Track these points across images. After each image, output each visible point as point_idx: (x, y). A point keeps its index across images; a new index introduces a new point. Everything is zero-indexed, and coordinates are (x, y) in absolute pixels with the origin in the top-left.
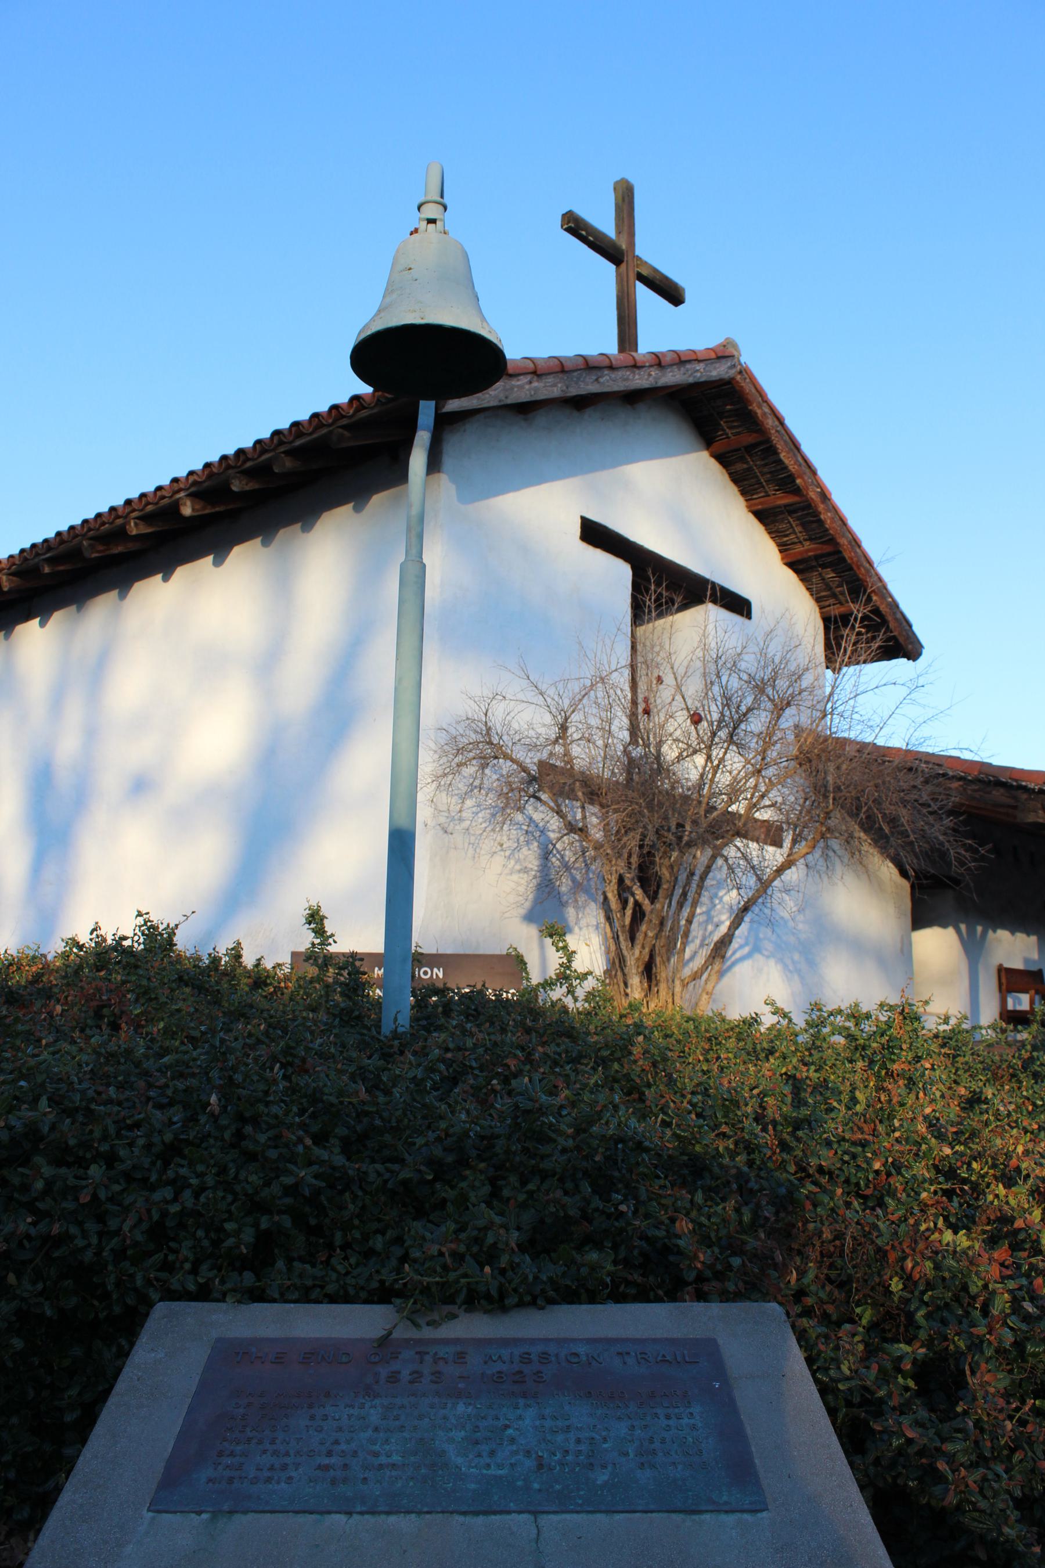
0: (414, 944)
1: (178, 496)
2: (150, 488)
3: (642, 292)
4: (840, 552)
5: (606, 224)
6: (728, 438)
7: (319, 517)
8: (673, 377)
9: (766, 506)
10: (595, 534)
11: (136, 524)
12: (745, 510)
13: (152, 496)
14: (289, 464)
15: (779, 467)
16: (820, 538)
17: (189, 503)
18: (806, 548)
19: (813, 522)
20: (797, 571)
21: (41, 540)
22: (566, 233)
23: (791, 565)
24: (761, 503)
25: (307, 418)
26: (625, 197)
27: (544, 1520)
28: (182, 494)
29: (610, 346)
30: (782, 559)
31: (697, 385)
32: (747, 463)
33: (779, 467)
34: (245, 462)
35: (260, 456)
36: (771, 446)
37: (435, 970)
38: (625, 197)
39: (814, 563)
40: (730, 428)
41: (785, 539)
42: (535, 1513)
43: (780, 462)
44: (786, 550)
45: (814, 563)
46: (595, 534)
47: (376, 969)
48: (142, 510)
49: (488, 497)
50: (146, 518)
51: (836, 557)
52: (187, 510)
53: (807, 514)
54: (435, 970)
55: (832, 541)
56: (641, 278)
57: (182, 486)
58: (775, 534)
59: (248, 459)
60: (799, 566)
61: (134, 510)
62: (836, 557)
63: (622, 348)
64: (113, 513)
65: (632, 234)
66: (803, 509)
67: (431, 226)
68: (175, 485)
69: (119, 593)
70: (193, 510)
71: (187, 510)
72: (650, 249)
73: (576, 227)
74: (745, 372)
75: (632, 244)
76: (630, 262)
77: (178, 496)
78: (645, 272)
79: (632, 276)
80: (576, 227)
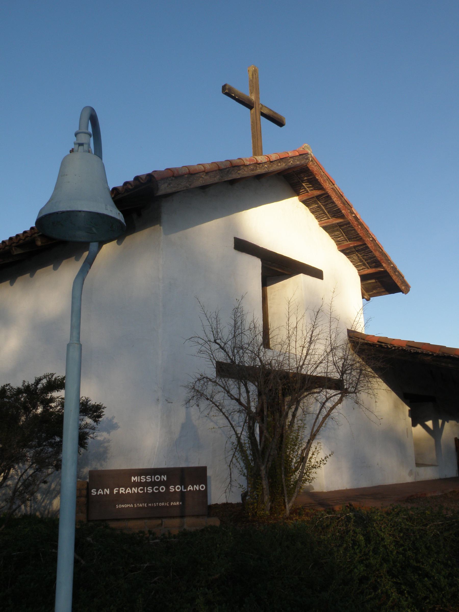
0: (427, 474)
1: (34, 236)
2: (21, 232)
4: (365, 244)
6: (308, 192)
7: (60, 265)
9: (328, 224)
12: (319, 226)
13: (21, 236)
14: (19, 251)
15: (333, 205)
16: (356, 238)
17: (39, 239)
18: (351, 244)
19: (352, 230)
20: (346, 254)
21: (15, 235)
22: (225, 95)
23: (343, 251)
24: (326, 223)
25: (29, 229)
28: (36, 235)
30: (338, 248)
31: (290, 169)
32: (318, 204)
33: (333, 205)
36: (329, 196)
37: (163, 476)
39: (354, 250)
40: (308, 187)
41: (339, 239)
43: (333, 203)
44: (340, 244)
45: (354, 250)
47: (133, 478)
48: (17, 243)
49: (188, 228)
50: (19, 246)
51: (364, 246)
52: (39, 243)
53: (349, 227)
54: (163, 476)
55: (360, 239)
56: (263, 114)
57: (36, 231)
58: (334, 238)
60: (346, 252)
61: (14, 243)
62: (364, 246)
64: (4, 244)
65: (257, 93)
66: (346, 224)
67: (81, 148)
68: (33, 230)
69: (117, 243)
70: (42, 243)
71: (39, 243)
73: (228, 92)
75: (258, 98)
76: (257, 107)
77: (34, 236)
78: (265, 111)
79: (258, 114)
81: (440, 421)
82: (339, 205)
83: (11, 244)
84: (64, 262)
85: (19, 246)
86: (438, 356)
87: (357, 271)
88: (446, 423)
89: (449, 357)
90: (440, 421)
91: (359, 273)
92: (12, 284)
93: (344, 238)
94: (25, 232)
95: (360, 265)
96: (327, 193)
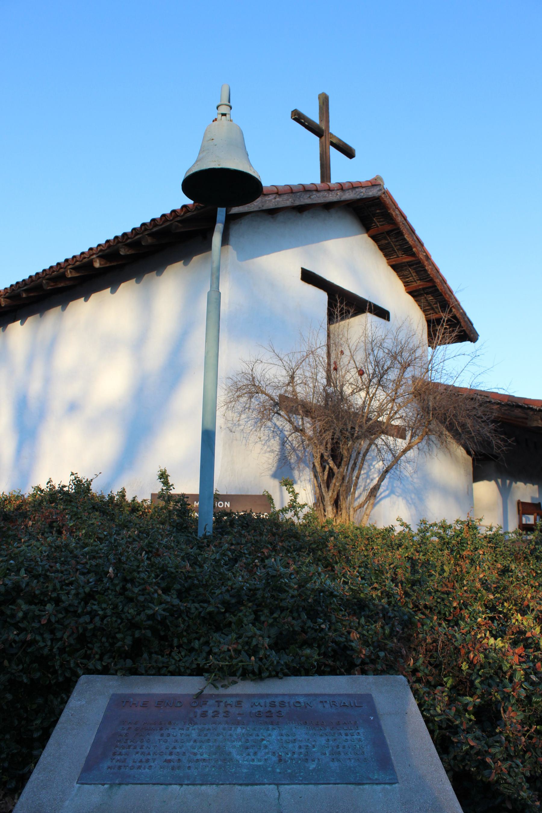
3: (333, 151)
4: (435, 286)
5: (314, 116)
6: (378, 227)
7: (165, 268)
8: (349, 196)
9: (397, 262)
10: (309, 277)
11: (71, 272)
13: (79, 257)
14: (150, 240)
15: (404, 242)
16: (426, 279)
17: (98, 261)
19: (422, 271)
20: (413, 296)
22: (293, 121)
23: (410, 293)
26: (324, 102)
27: (282, 788)
28: (94, 256)
29: (316, 179)
30: (406, 290)
31: (361, 200)
32: (387, 240)
33: (404, 242)
34: (127, 240)
35: (135, 236)
36: (400, 231)
38: (324, 102)
39: (422, 292)
41: (407, 279)
42: (278, 785)
43: (405, 239)
44: (408, 285)
45: (422, 292)
46: (309, 277)
48: (74, 264)
52: (97, 265)
56: (333, 144)
59: (129, 238)
60: (414, 293)
61: (70, 265)
62: (434, 289)
63: (323, 180)
64: (59, 266)
65: (328, 122)
66: (416, 264)
68: (91, 251)
70: (100, 264)
71: (97, 265)
72: (337, 129)
73: (299, 118)
74: (386, 193)
79: (328, 143)
80: (299, 118)
81: (508, 482)
82: (410, 242)
83: (67, 266)
84: (146, 276)
85: (130, 246)
86: (507, 405)
87: (424, 316)
88: (514, 483)
89: (518, 406)
90: (508, 482)
91: (426, 318)
92: (86, 300)
93: (414, 279)
94: (44, 270)
95: (428, 309)
96: (399, 228)
